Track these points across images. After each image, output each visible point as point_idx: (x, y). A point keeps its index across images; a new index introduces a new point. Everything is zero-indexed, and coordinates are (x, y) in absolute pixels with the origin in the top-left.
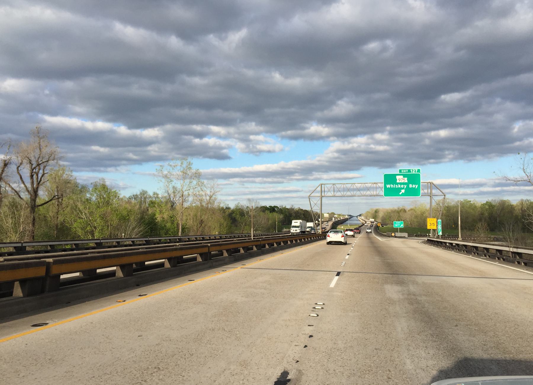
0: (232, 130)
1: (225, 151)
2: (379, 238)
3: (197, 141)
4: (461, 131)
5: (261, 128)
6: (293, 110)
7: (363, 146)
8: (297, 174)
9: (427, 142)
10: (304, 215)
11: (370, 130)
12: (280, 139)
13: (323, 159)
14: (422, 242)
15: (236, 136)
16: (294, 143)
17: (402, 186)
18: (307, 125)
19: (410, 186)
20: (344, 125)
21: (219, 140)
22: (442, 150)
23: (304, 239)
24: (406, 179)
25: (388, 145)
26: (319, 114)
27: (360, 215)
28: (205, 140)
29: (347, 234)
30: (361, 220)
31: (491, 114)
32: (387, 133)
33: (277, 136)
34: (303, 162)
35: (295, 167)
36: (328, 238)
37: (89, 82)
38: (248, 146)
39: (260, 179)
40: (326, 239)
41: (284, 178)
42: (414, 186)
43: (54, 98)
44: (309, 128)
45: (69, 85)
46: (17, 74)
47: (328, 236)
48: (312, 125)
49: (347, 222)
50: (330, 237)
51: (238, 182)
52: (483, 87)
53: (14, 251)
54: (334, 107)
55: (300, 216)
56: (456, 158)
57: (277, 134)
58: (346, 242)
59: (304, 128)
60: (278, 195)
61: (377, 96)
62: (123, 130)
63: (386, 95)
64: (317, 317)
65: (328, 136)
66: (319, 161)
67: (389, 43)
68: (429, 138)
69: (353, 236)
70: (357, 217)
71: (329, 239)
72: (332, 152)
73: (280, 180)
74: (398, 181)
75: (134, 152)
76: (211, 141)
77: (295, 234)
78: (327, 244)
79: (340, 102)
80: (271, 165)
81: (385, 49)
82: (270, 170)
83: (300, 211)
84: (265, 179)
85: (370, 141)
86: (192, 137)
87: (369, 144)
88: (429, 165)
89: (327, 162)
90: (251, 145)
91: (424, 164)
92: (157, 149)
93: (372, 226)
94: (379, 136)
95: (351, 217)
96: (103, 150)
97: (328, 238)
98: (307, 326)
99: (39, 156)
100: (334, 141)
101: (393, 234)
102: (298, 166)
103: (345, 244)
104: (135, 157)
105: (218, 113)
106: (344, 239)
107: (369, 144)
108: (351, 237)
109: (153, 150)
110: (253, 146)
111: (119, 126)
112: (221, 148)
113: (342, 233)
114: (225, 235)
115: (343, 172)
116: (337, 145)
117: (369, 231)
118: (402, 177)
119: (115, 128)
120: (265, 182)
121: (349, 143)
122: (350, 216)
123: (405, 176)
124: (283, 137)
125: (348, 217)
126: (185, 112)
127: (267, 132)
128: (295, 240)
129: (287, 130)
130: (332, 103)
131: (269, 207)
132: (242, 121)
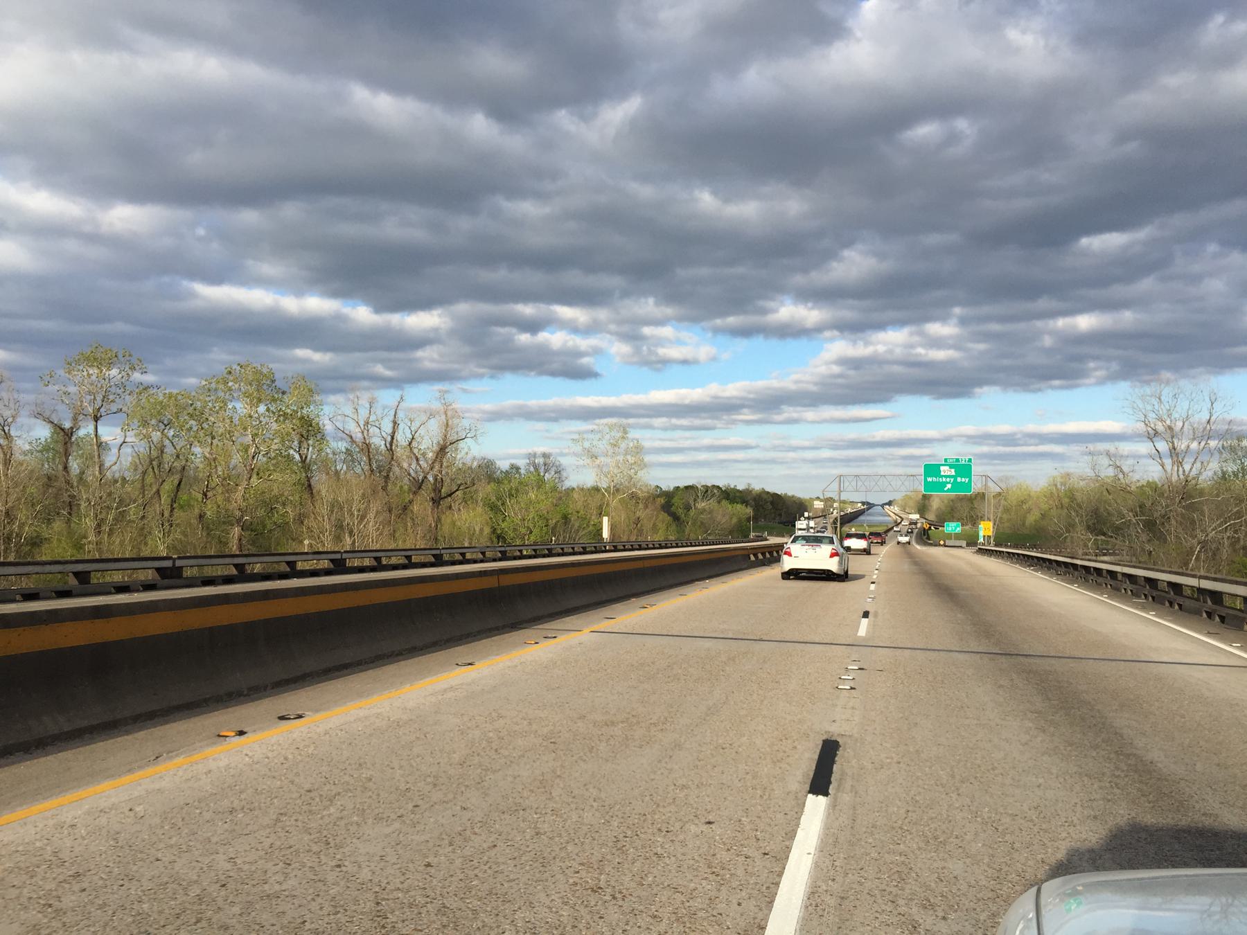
0: (602, 314)
1: (585, 361)
2: (918, 547)
3: (524, 338)
4: (1127, 317)
5: (669, 311)
6: (740, 270)
7: (898, 351)
8: (745, 410)
9: (1048, 341)
10: (772, 503)
11: (916, 315)
12: (710, 335)
13: (807, 378)
14: (975, 553)
15: (613, 327)
16: (742, 344)
17: (948, 480)
18: (771, 304)
19: (959, 479)
20: (856, 303)
21: (573, 336)
22: (1081, 358)
23: (762, 554)
24: (953, 470)
25: (956, 347)
26: (799, 279)
27: (890, 503)
28: (543, 336)
29: (848, 549)
30: (892, 514)
31: (1196, 279)
32: (954, 321)
33: (703, 329)
34: (761, 384)
35: (744, 394)
36: (785, 557)
37: (291, 211)
38: (637, 351)
39: (664, 420)
40: (780, 561)
41: (717, 418)
42: (963, 480)
43: (215, 245)
44: (775, 311)
45: (249, 217)
46: (138, 194)
47: (786, 553)
48: (782, 304)
49: (862, 518)
50: (793, 555)
52: (1180, 221)
53: (332, 566)
54: (835, 264)
55: (765, 507)
56: (1114, 377)
57: (704, 324)
58: (846, 573)
59: (765, 312)
60: (703, 456)
61: (933, 239)
62: (362, 314)
63: (952, 238)
65: (818, 329)
66: (796, 382)
67: (962, 124)
68: (1051, 333)
69: (867, 552)
70: (882, 506)
71: (788, 563)
72: (828, 363)
73: (709, 422)
74: (942, 473)
75: (385, 362)
76: (555, 339)
78: (783, 578)
79: (846, 253)
81: (952, 138)
82: (687, 402)
83: (765, 496)
84: (674, 421)
85: (916, 339)
86: (514, 330)
87: (912, 346)
88: (1050, 392)
89: (816, 384)
90: (645, 348)
91: (1040, 390)
92: (435, 356)
93: (912, 532)
94: (936, 329)
95: (870, 506)
96: (319, 358)
97: (785, 557)
100: (832, 339)
101: (942, 543)
102: (749, 392)
103: (843, 577)
104: (388, 373)
105: (573, 278)
106: (840, 563)
107: (912, 346)
108: (859, 553)
109: (428, 357)
110: (649, 349)
111: (354, 307)
112: (579, 354)
113: (834, 543)
114: (593, 545)
115: (850, 407)
116: (839, 347)
117: (904, 539)
118: (947, 468)
120: (675, 428)
121: (867, 343)
122: (868, 503)
123: (951, 467)
124: (717, 331)
125: (862, 507)
126: (500, 275)
127: (680, 319)
128: (769, 552)
129: (724, 314)
130: (829, 255)
131: (702, 486)
132: (626, 294)
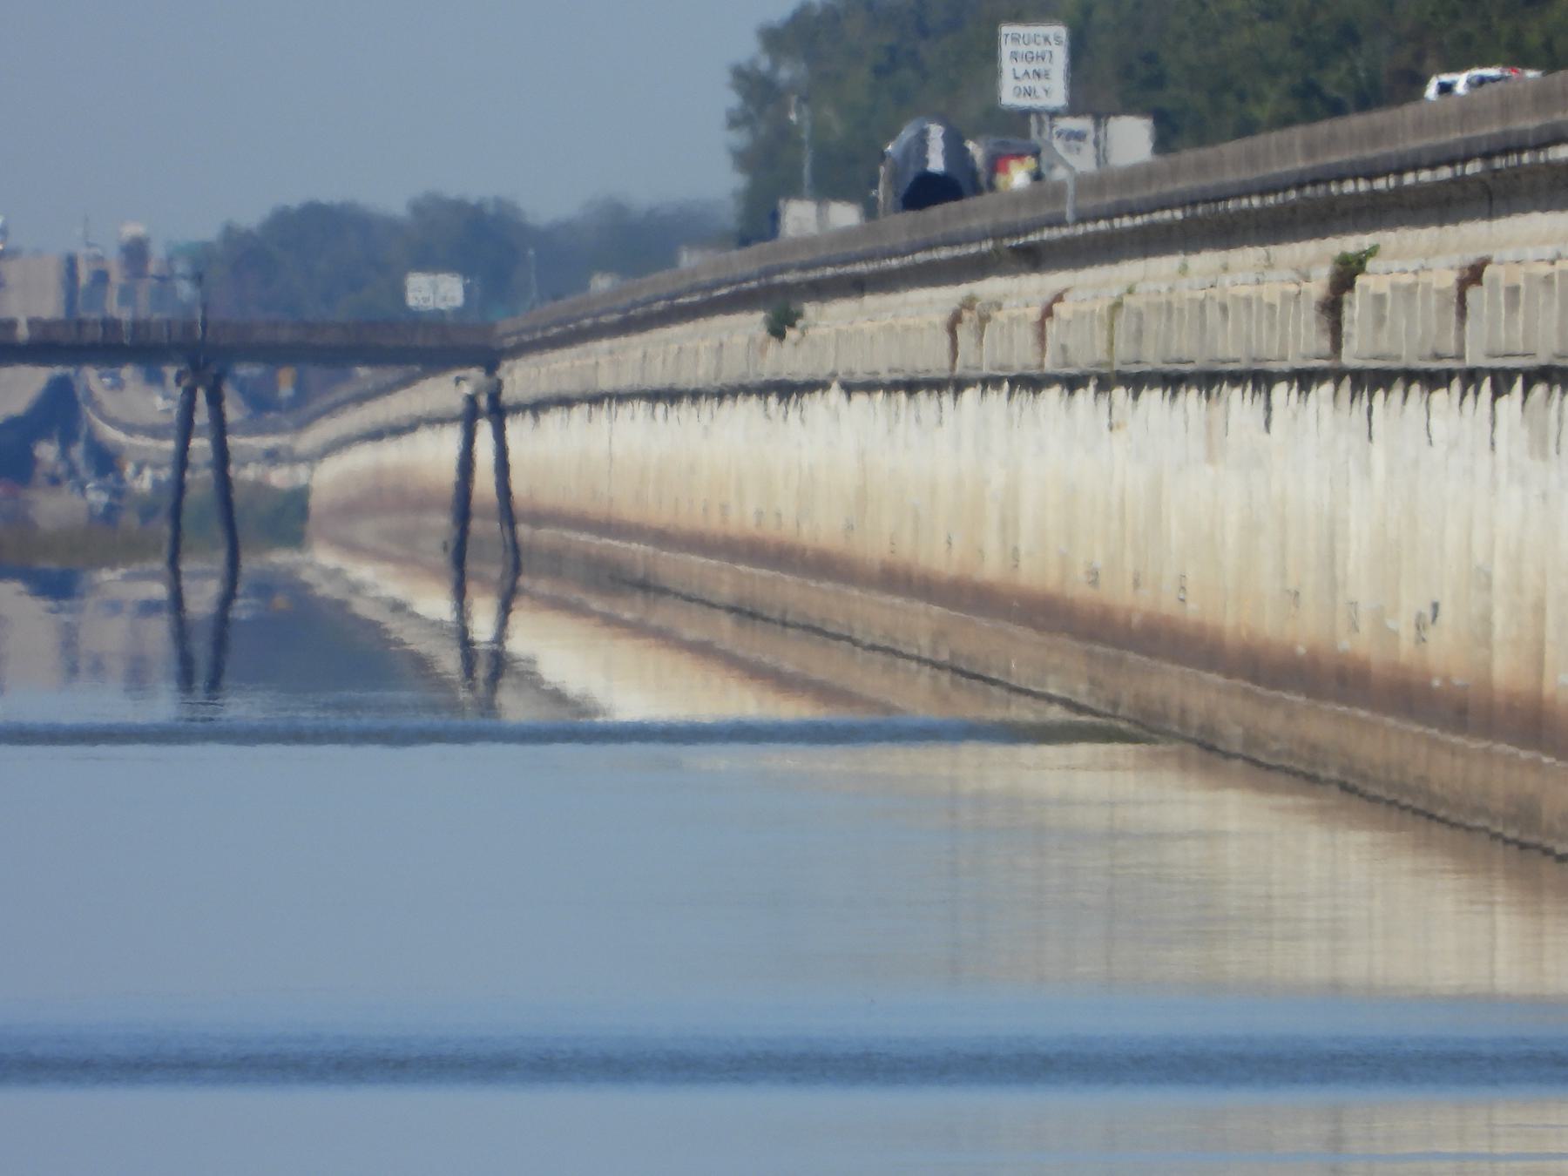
51: (1487, 619)
64: (1012, 76)
77: (724, 291)
80: (778, 572)
98: (1012, 67)
99: (776, 615)
119: (806, 147)
127: (1456, 872)
